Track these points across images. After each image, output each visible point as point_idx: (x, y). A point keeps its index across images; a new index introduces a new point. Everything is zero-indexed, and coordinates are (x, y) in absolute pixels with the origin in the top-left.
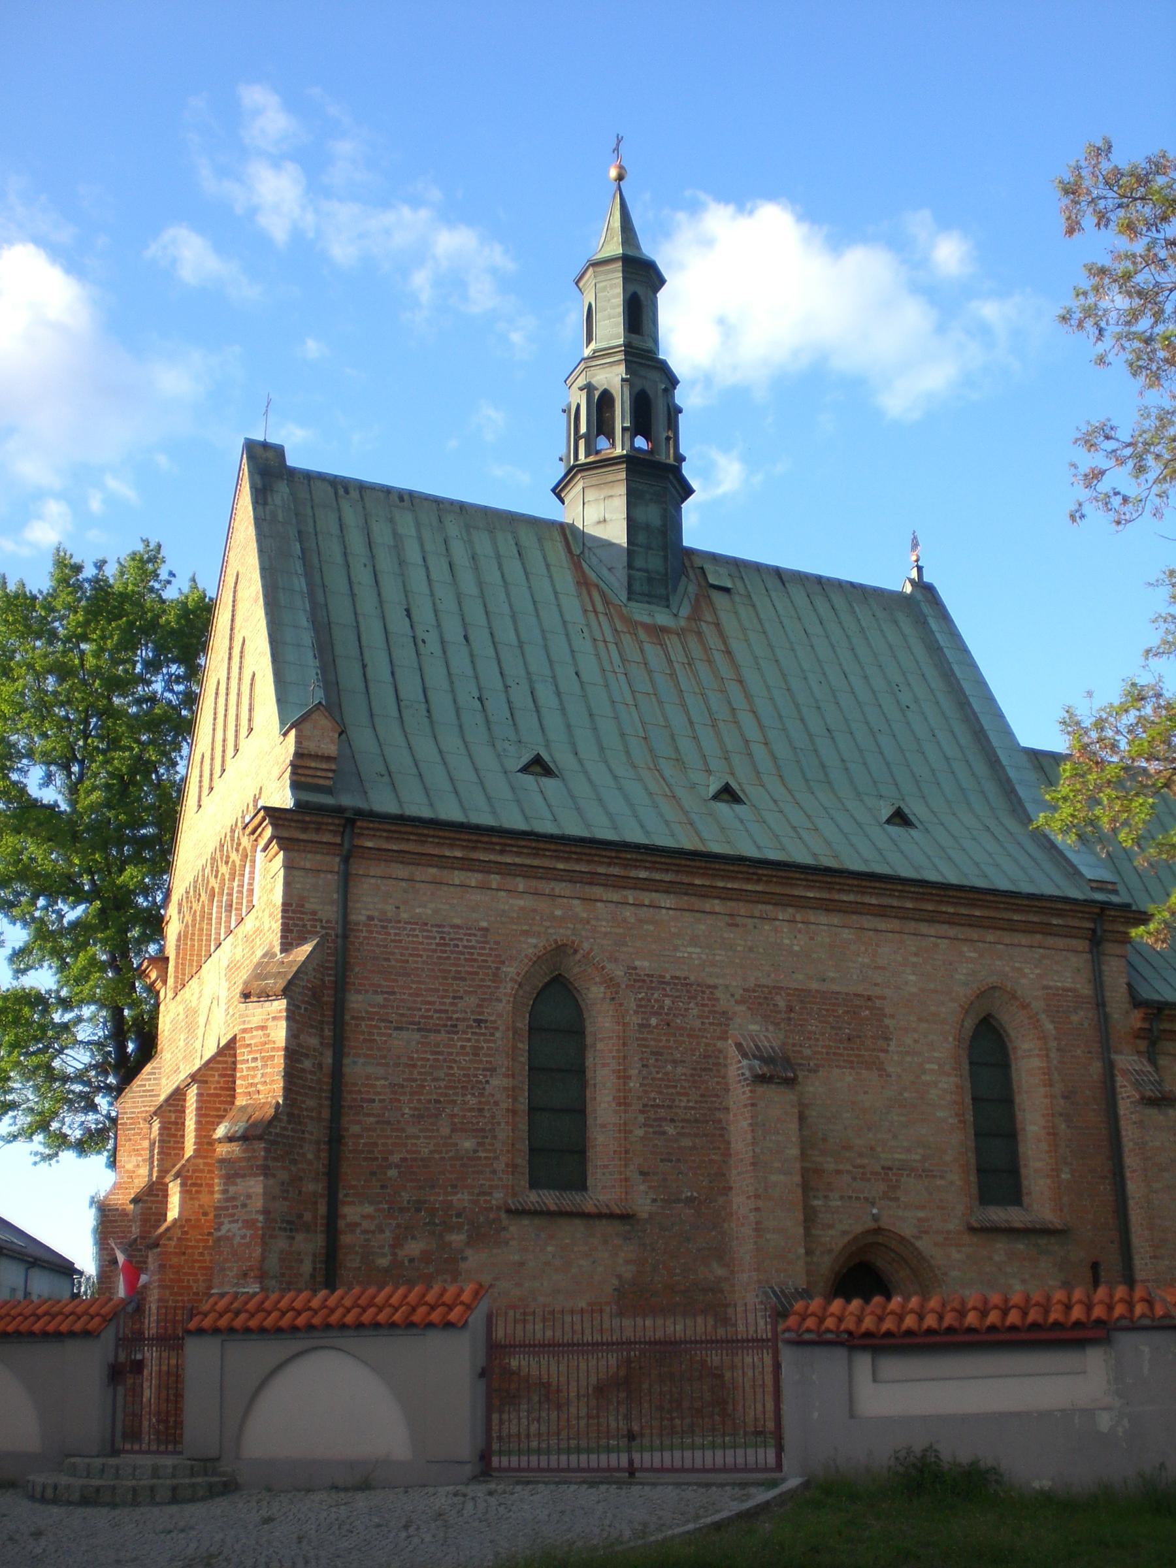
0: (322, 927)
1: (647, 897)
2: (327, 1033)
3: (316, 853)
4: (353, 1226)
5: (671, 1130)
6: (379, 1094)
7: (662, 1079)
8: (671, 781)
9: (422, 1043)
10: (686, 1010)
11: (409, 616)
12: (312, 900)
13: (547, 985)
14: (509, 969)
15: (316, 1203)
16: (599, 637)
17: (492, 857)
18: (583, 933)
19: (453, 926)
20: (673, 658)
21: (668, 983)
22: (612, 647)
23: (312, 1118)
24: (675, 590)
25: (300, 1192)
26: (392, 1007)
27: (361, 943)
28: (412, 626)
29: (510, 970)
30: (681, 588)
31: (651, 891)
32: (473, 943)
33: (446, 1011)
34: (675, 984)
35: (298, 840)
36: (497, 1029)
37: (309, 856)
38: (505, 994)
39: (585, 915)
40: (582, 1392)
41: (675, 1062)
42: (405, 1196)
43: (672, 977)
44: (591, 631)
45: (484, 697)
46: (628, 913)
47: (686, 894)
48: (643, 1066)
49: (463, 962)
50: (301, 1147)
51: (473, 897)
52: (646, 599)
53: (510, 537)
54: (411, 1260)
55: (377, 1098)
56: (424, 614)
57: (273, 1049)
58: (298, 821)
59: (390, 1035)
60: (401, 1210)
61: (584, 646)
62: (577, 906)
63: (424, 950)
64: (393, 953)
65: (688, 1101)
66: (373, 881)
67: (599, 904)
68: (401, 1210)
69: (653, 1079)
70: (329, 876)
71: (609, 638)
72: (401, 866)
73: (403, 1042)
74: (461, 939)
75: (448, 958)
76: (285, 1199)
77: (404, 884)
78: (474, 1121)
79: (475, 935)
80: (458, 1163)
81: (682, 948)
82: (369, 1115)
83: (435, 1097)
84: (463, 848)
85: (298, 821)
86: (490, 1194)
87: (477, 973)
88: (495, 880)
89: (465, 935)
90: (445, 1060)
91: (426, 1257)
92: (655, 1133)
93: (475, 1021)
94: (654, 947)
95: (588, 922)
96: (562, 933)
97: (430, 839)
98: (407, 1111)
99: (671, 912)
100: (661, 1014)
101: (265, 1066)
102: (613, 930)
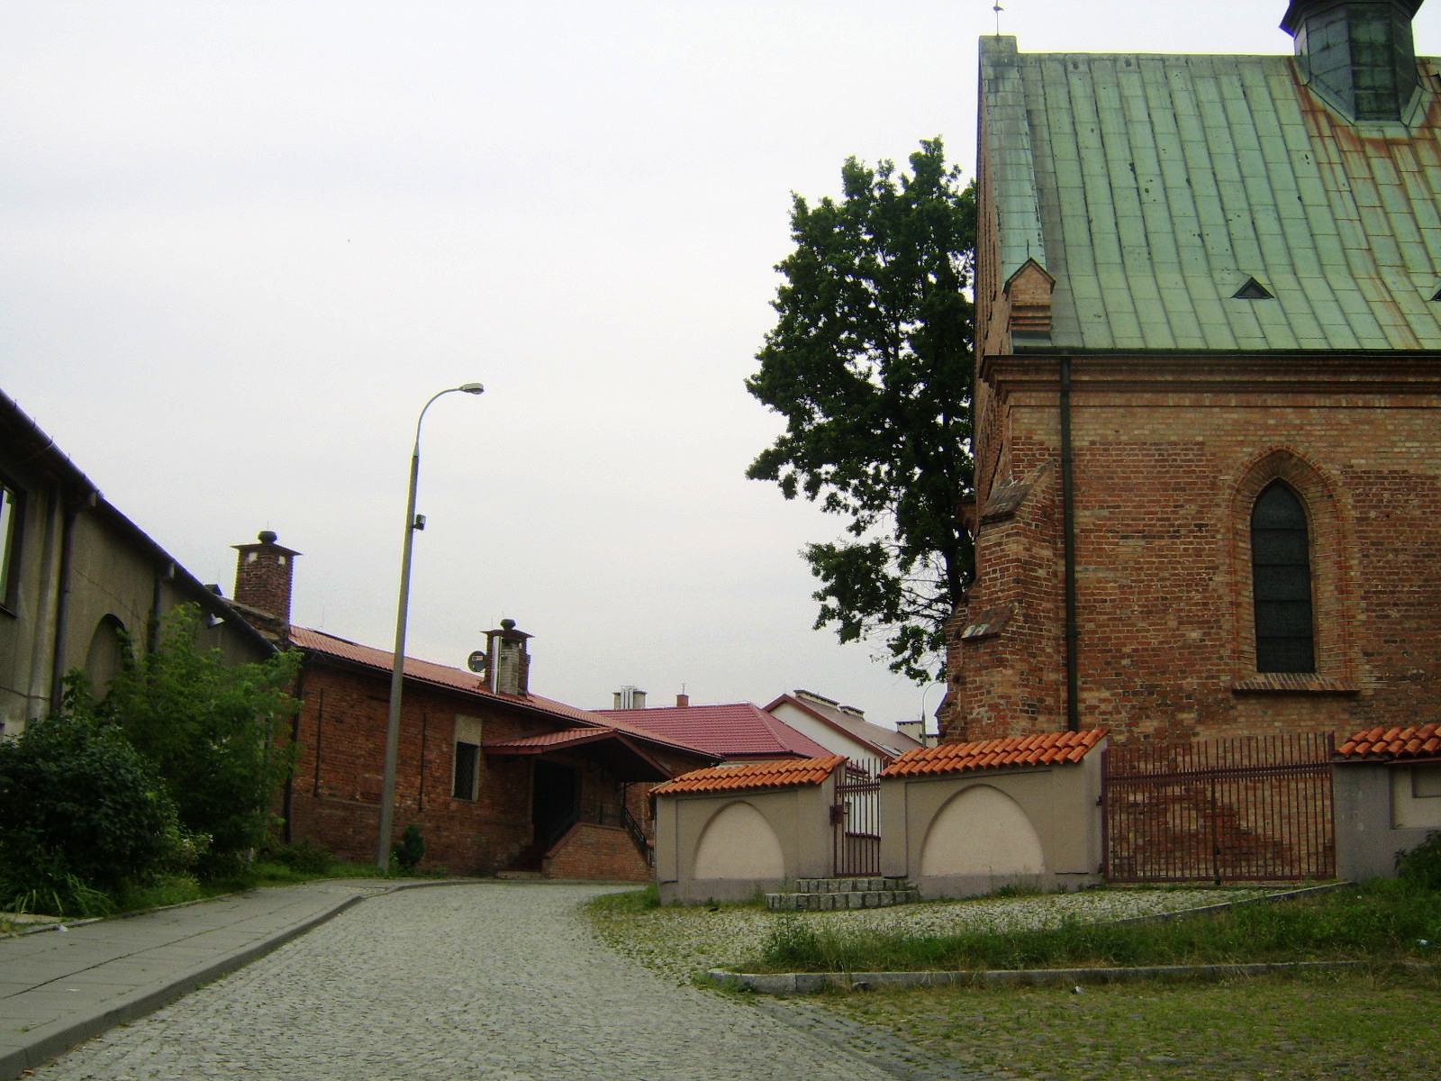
0: (1050, 455)
1: (1359, 400)
2: (1060, 545)
3: (1047, 391)
4: (1092, 709)
5: (1394, 614)
6: (1111, 594)
7: (1384, 568)
8: (1391, 286)
9: (1147, 548)
10: (1407, 501)
11: (1133, 170)
12: (1039, 432)
13: (1266, 490)
14: (1226, 477)
15: (1058, 690)
16: (1323, 159)
17: (1202, 378)
18: (1297, 438)
19: (1171, 443)
20: (1402, 168)
21: (1385, 478)
22: (1338, 169)
23: (1049, 618)
24: (1407, 101)
25: (1041, 680)
26: (1118, 519)
27: (1086, 466)
28: (1136, 179)
29: (1227, 478)
30: (1414, 99)
31: (1364, 393)
32: (1191, 457)
33: (1169, 519)
34: (1393, 478)
35: (1021, 381)
36: (1218, 531)
37: (1034, 394)
38: (1224, 500)
39: (1298, 422)
40: (1312, 850)
41: (1396, 551)
42: (1138, 682)
43: (1390, 472)
44: (1315, 157)
45: (1205, 232)
46: (1342, 416)
47: (1402, 393)
48: (1364, 556)
49: (1181, 474)
50: (1040, 643)
51: (1188, 415)
52: (1375, 115)
53: (1235, 78)
54: (1146, 737)
55: (1108, 598)
56: (1147, 166)
57: (1008, 561)
58: (1018, 365)
59: (1117, 544)
60: (1135, 694)
61: (1307, 170)
62: (1292, 416)
63: (1145, 466)
64: (1115, 472)
65: (1411, 586)
66: (1093, 410)
67: (1312, 410)
68: (1135, 694)
69: (1374, 568)
70: (1052, 410)
71: (1335, 158)
72: (1118, 395)
73: (1130, 548)
74: (1179, 454)
75: (1167, 472)
76: (1026, 686)
77: (1121, 410)
78: (1200, 614)
79: (1192, 450)
80: (1186, 651)
81: (1399, 444)
82: (1101, 613)
83: (1161, 594)
84: (1172, 372)
85: (1018, 365)
86: (1218, 678)
87: (1195, 483)
88: (1207, 399)
89: (1182, 450)
90: (1170, 562)
91: (1159, 733)
92: (1377, 617)
93: (1196, 525)
94: (1370, 444)
95: (1302, 429)
96: (1277, 441)
97: (1142, 368)
98: (1136, 608)
99: (1386, 411)
100: (1380, 507)
101: (1002, 577)
102: (1328, 433)
